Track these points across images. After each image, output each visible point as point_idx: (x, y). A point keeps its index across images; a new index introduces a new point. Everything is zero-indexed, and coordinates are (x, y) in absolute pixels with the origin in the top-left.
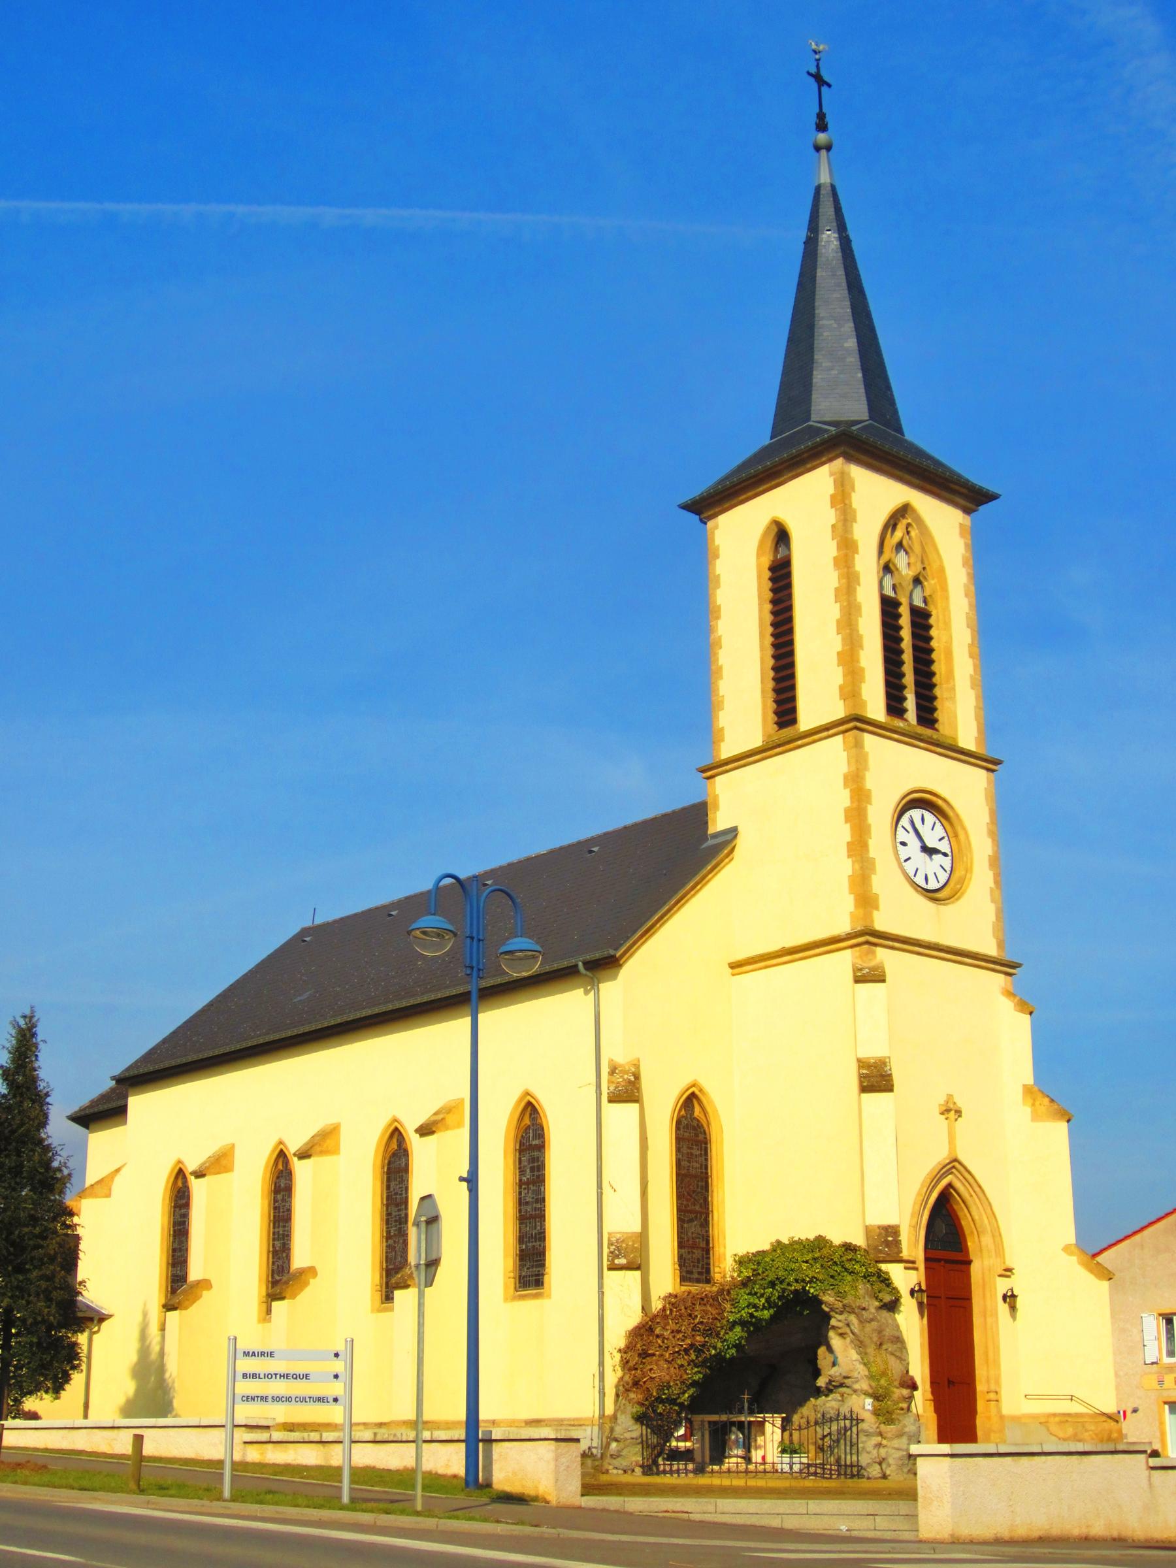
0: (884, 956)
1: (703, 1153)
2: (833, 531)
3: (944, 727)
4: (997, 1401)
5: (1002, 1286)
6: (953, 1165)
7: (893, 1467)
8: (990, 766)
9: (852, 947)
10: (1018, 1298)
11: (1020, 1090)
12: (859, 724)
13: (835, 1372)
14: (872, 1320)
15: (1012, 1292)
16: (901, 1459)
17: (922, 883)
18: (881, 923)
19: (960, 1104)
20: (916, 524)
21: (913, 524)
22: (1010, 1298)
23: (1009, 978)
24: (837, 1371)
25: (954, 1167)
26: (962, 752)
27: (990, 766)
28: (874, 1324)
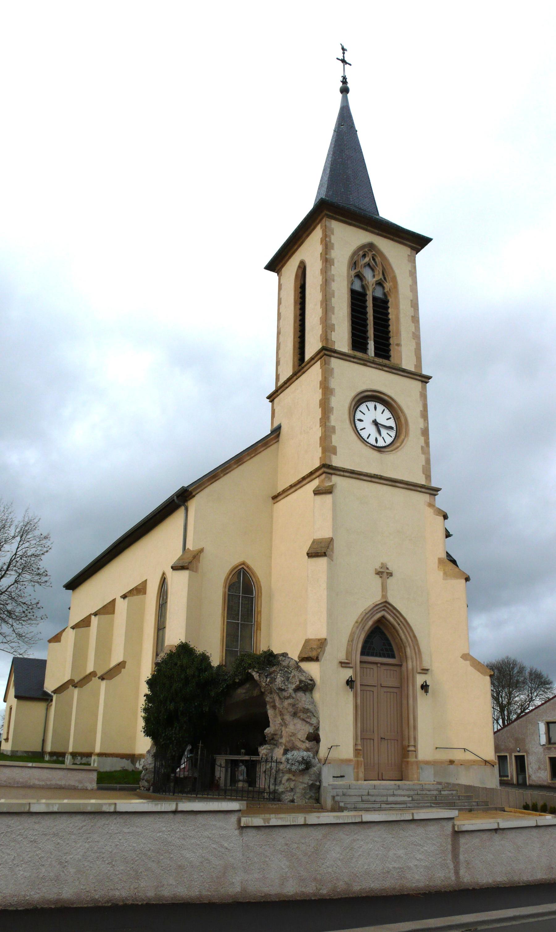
0: (335, 479)
1: (250, 602)
2: (321, 256)
3: (394, 360)
4: (415, 751)
5: (420, 680)
6: (164, 571)
7: (298, 795)
8: (423, 379)
9: (318, 476)
10: (430, 687)
11: (437, 561)
12: (326, 352)
13: (268, 731)
14: (288, 698)
15: (426, 683)
16: (304, 789)
17: (374, 443)
18: (336, 462)
19: (391, 569)
20: (378, 254)
21: (377, 255)
22: (425, 687)
23: (328, 463)
24: (269, 730)
25: (385, 606)
26: (404, 371)
27: (423, 379)
28: (290, 701)
